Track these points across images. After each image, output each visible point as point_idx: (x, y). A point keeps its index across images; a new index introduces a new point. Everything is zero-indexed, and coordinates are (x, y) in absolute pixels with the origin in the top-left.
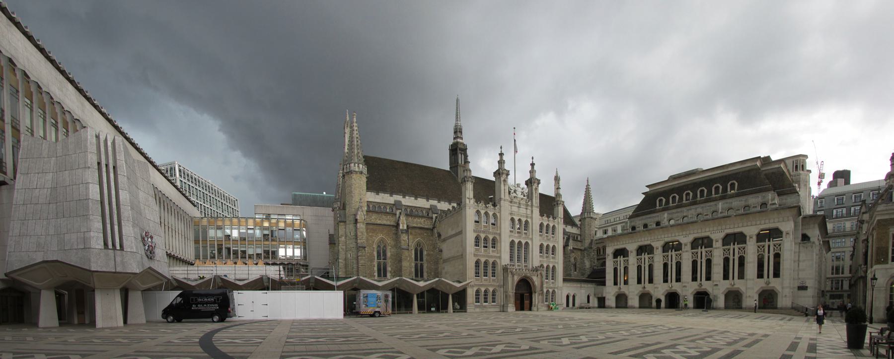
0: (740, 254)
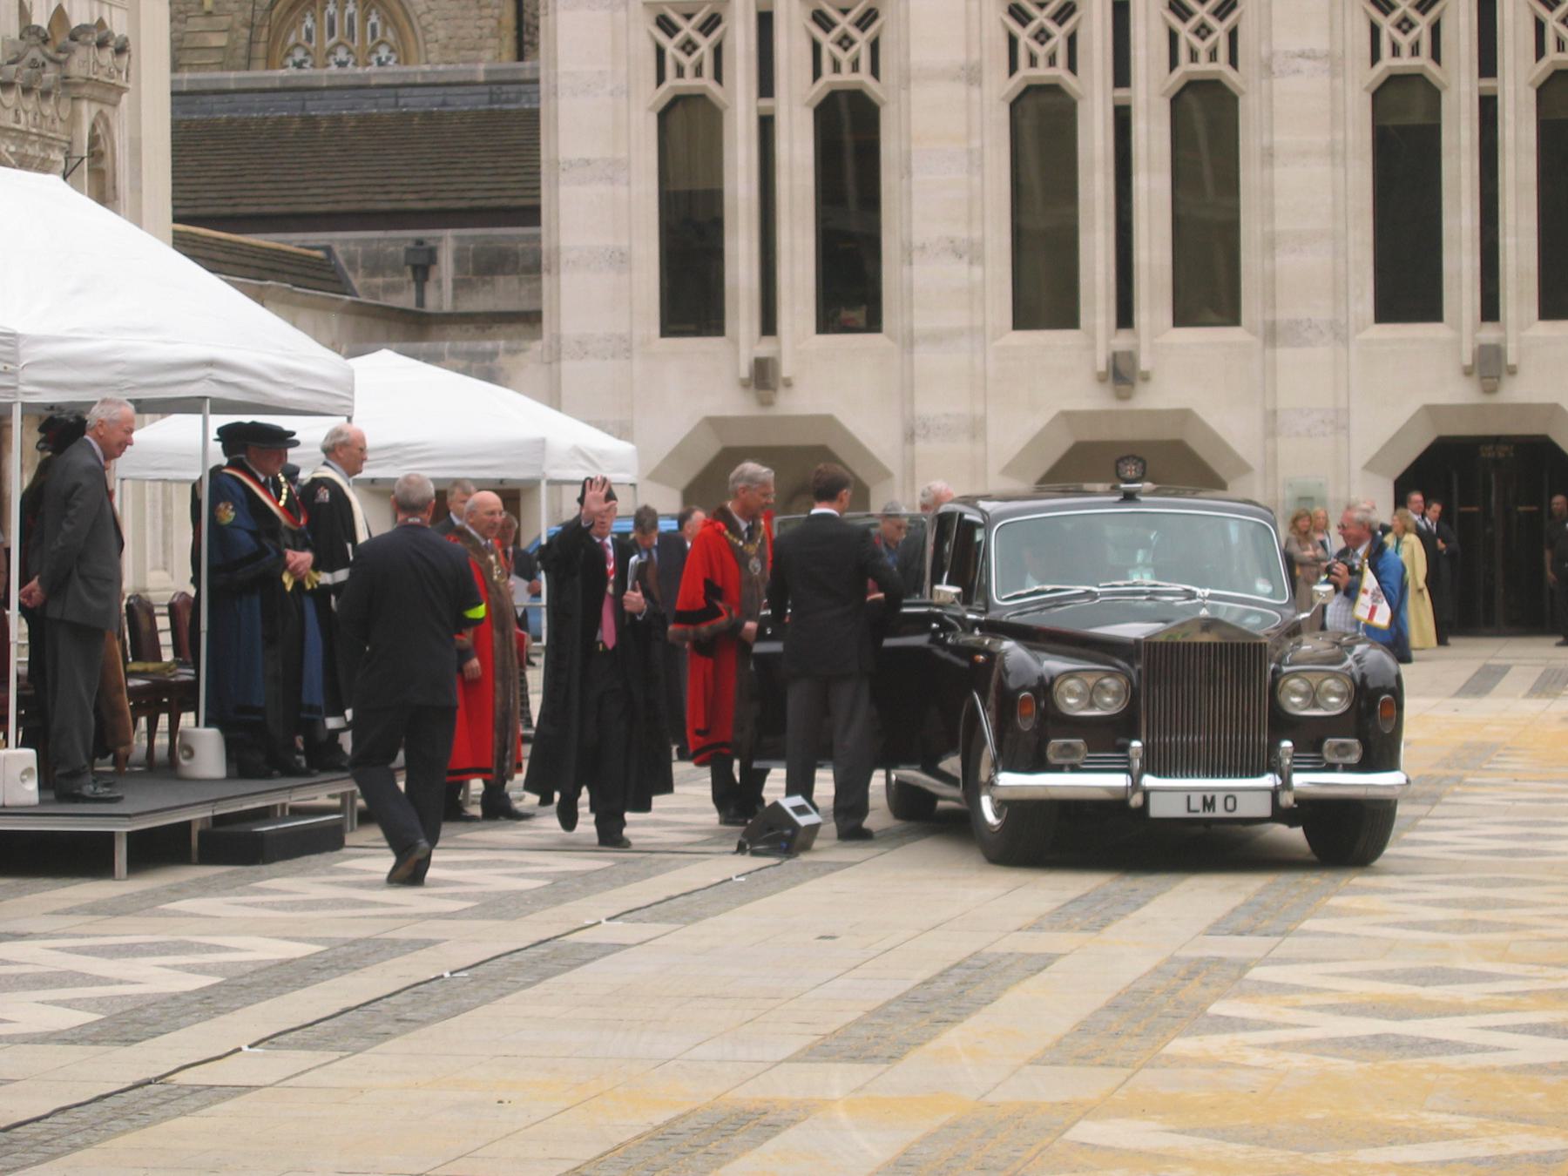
0: (1387, 62)
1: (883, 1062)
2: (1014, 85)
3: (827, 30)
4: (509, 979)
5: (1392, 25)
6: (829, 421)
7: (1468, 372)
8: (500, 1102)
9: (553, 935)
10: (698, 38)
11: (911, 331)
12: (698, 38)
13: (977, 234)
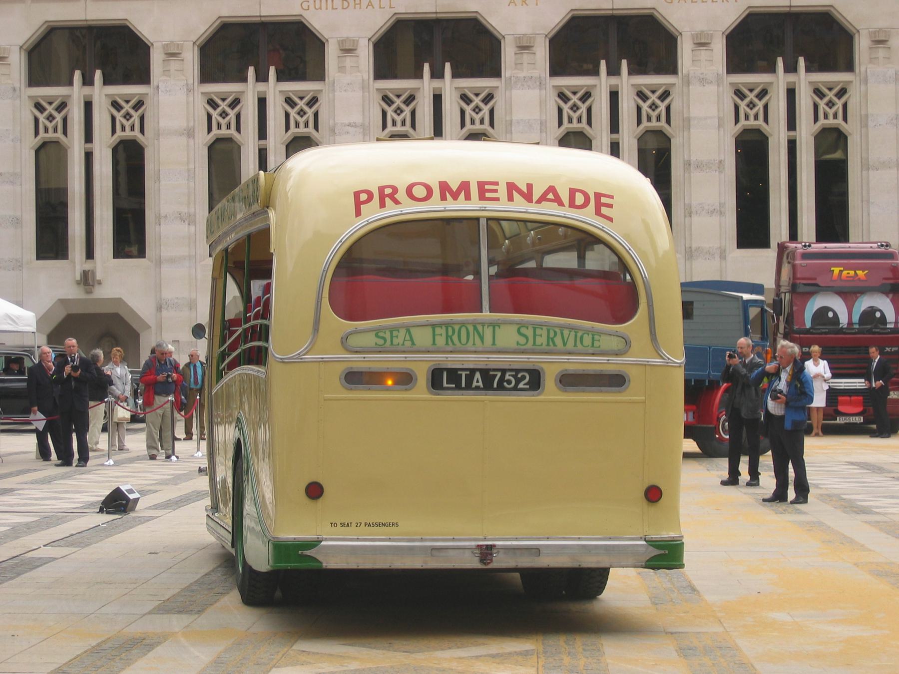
0: (822, 121)
1: (196, 614)
2: (210, 138)
3: (293, 107)
4: (2, 575)
5: (392, 111)
6: (119, 301)
7: (78, 283)
8: (13, 636)
9: (18, 554)
10: (55, 114)
11: (160, 256)
12: (55, 114)
13: (192, 210)
